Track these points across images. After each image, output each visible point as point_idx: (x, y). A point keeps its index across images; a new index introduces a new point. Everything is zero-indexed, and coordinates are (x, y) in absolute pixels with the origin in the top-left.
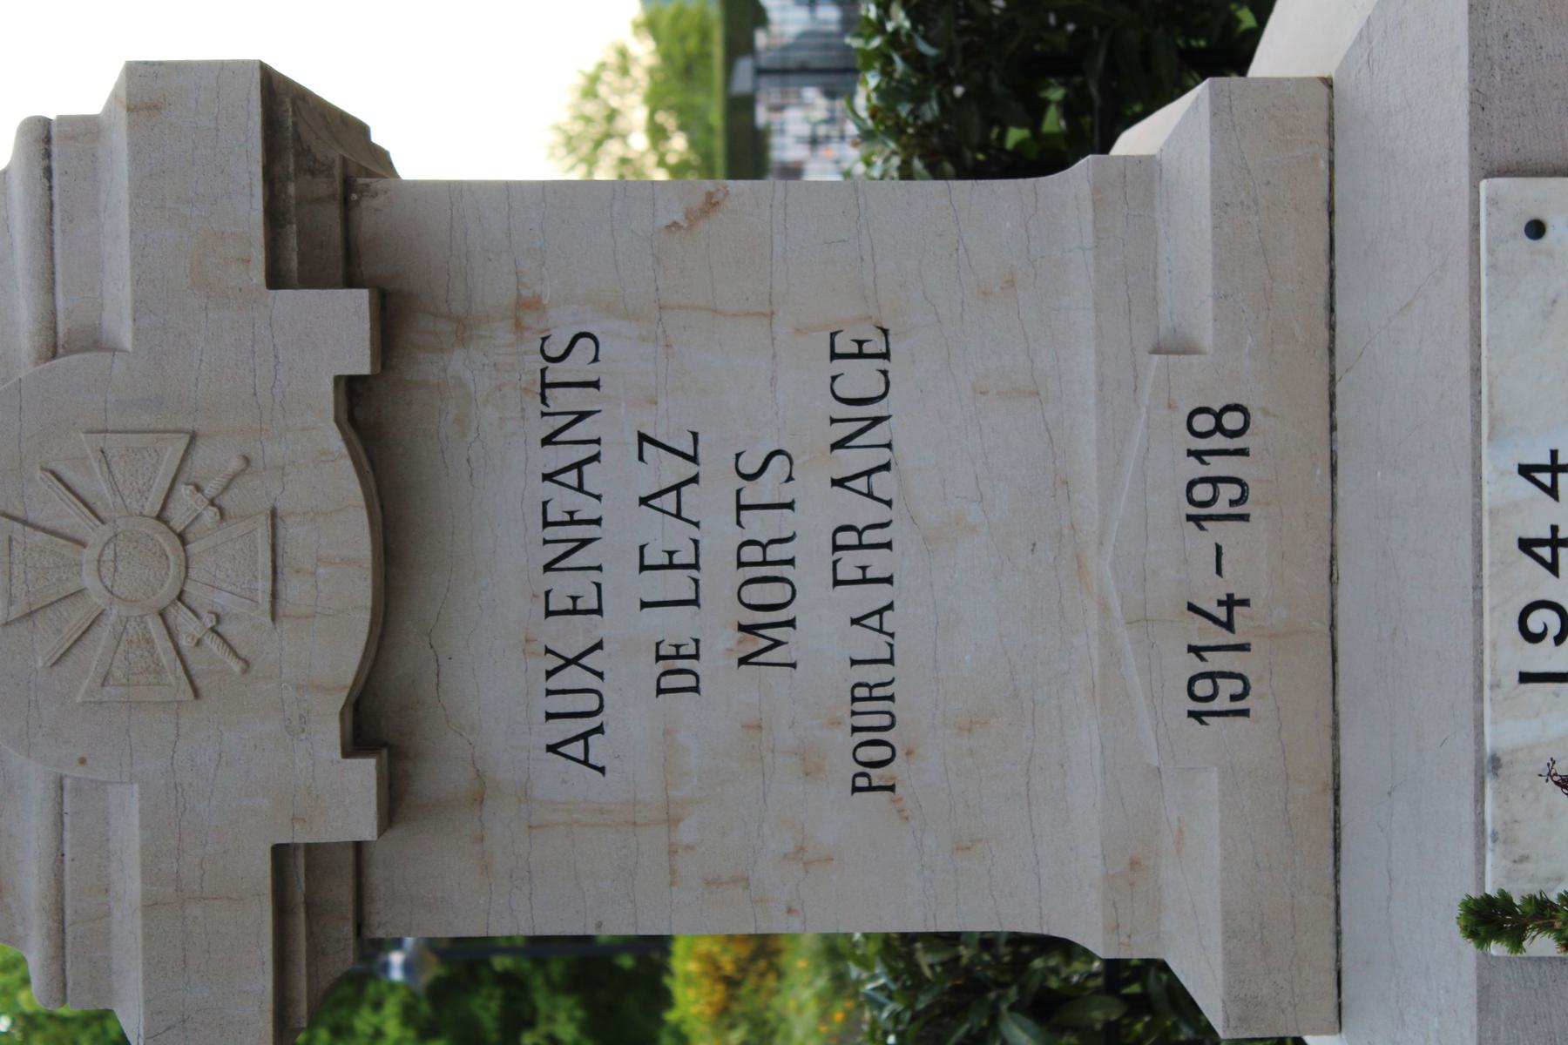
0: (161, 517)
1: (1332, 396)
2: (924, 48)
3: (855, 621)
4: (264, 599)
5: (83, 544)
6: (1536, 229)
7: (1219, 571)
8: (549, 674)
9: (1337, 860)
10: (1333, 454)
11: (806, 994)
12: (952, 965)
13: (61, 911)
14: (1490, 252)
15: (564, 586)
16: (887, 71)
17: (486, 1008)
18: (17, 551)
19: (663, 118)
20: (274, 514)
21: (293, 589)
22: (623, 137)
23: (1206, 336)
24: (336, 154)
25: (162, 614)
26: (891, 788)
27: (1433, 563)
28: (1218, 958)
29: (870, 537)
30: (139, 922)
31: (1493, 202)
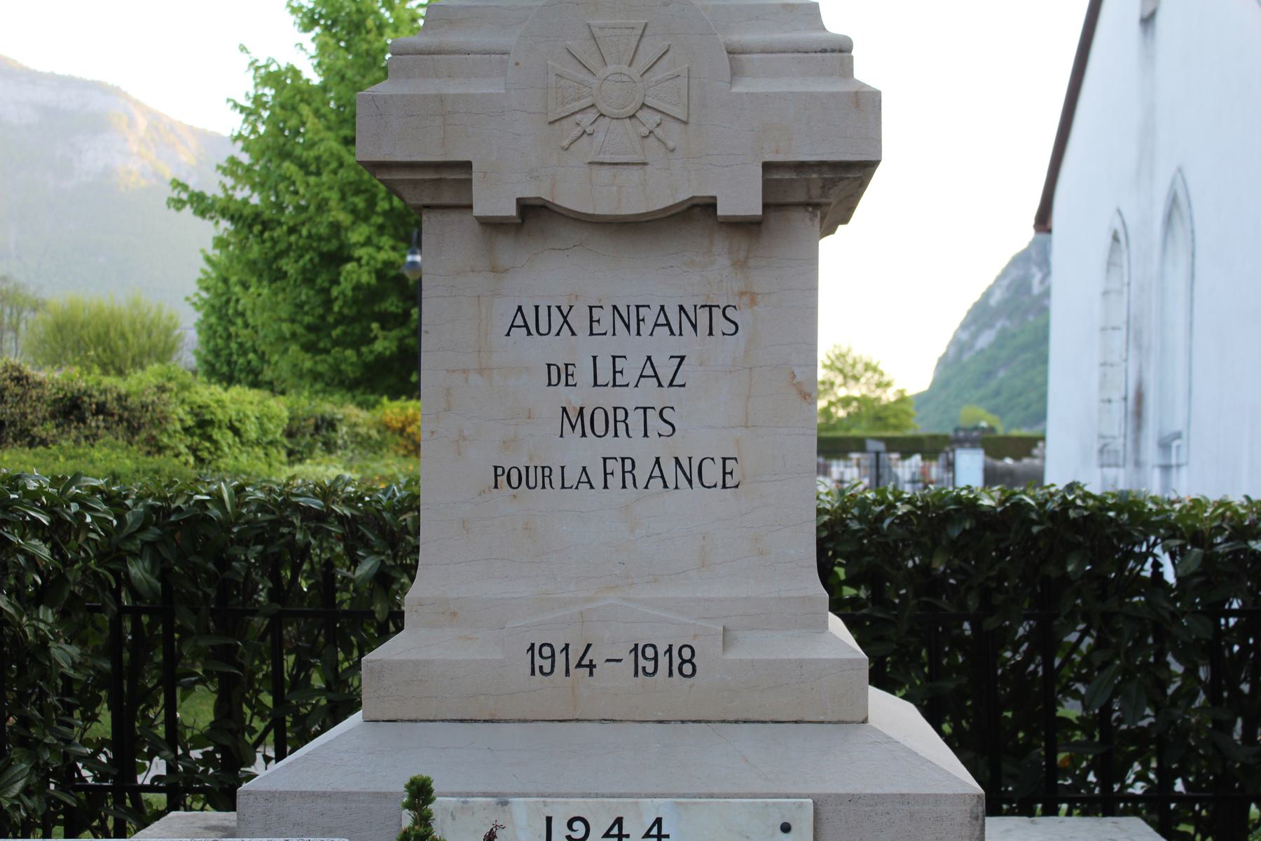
0: (643, 105)
1: (700, 722)
2: (887, 522)
3: (584, 469)
4: (600, 158)
5: (630, 65)
6: (786, 828)
7: (608, 660)
8: (559, 308)
9: (455, 721)
10: (669, 722)
11: (395, 469)
12: (405, 529)
13: (439, 53)
14: (775, 804)
15: (605, 316)
16: (875, 502)
17: (391, 305)
18: (627, 31)
19: (855, 404)
20: (644, 164)
21: (605, 173)
22: (845, 384)
23: (732, 655)
24: (833, 200)
25: (593, 105)
26: (496, 487)
27: (611, 775)
28: (403, 657)
29: (629, 477)
30: (434, 92)
31: (801, 805)
